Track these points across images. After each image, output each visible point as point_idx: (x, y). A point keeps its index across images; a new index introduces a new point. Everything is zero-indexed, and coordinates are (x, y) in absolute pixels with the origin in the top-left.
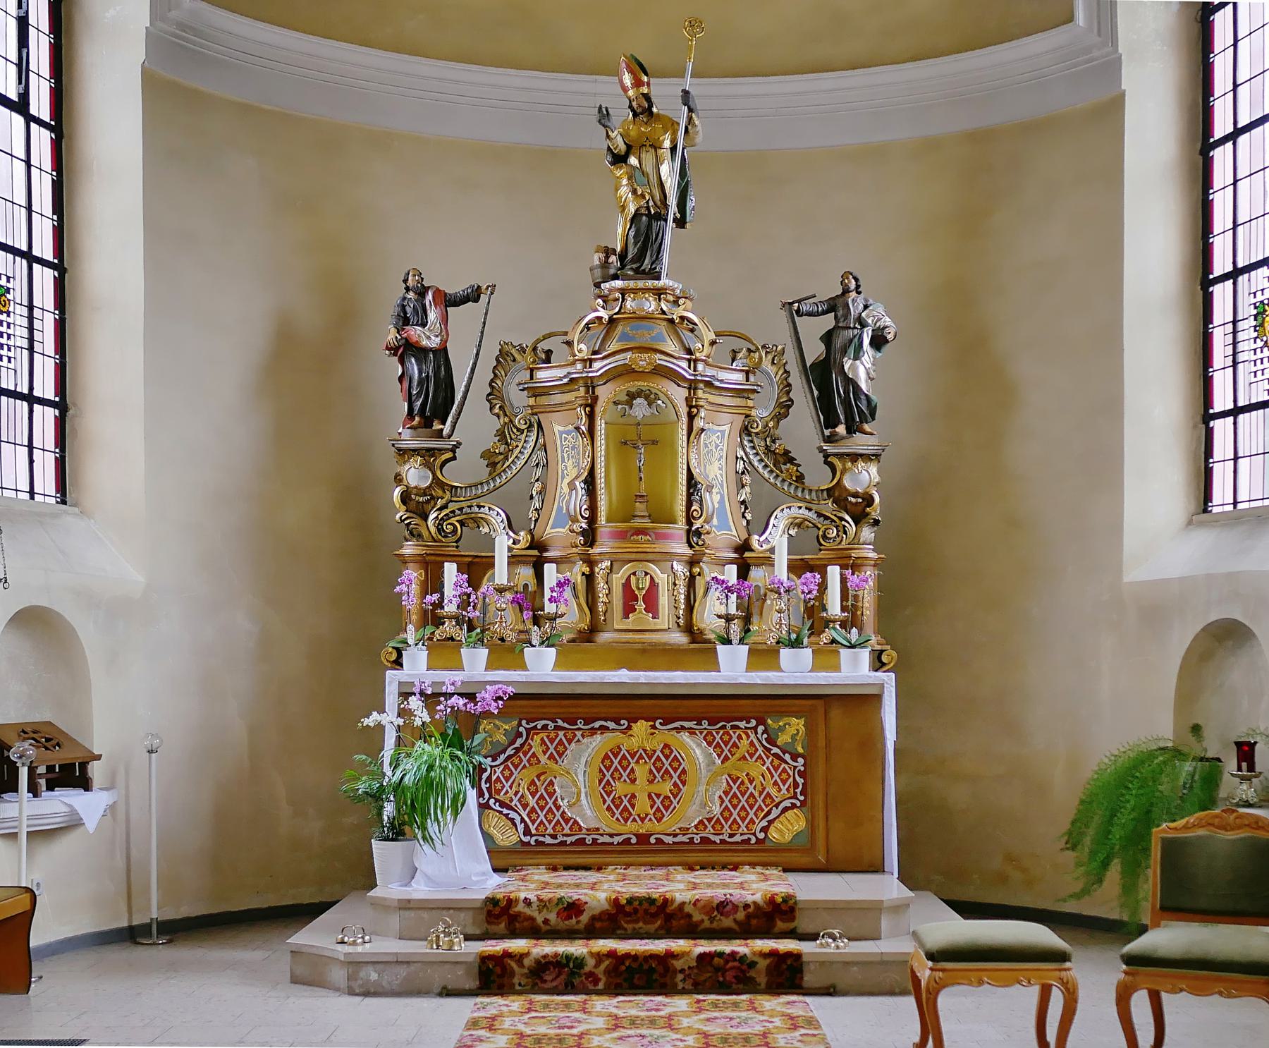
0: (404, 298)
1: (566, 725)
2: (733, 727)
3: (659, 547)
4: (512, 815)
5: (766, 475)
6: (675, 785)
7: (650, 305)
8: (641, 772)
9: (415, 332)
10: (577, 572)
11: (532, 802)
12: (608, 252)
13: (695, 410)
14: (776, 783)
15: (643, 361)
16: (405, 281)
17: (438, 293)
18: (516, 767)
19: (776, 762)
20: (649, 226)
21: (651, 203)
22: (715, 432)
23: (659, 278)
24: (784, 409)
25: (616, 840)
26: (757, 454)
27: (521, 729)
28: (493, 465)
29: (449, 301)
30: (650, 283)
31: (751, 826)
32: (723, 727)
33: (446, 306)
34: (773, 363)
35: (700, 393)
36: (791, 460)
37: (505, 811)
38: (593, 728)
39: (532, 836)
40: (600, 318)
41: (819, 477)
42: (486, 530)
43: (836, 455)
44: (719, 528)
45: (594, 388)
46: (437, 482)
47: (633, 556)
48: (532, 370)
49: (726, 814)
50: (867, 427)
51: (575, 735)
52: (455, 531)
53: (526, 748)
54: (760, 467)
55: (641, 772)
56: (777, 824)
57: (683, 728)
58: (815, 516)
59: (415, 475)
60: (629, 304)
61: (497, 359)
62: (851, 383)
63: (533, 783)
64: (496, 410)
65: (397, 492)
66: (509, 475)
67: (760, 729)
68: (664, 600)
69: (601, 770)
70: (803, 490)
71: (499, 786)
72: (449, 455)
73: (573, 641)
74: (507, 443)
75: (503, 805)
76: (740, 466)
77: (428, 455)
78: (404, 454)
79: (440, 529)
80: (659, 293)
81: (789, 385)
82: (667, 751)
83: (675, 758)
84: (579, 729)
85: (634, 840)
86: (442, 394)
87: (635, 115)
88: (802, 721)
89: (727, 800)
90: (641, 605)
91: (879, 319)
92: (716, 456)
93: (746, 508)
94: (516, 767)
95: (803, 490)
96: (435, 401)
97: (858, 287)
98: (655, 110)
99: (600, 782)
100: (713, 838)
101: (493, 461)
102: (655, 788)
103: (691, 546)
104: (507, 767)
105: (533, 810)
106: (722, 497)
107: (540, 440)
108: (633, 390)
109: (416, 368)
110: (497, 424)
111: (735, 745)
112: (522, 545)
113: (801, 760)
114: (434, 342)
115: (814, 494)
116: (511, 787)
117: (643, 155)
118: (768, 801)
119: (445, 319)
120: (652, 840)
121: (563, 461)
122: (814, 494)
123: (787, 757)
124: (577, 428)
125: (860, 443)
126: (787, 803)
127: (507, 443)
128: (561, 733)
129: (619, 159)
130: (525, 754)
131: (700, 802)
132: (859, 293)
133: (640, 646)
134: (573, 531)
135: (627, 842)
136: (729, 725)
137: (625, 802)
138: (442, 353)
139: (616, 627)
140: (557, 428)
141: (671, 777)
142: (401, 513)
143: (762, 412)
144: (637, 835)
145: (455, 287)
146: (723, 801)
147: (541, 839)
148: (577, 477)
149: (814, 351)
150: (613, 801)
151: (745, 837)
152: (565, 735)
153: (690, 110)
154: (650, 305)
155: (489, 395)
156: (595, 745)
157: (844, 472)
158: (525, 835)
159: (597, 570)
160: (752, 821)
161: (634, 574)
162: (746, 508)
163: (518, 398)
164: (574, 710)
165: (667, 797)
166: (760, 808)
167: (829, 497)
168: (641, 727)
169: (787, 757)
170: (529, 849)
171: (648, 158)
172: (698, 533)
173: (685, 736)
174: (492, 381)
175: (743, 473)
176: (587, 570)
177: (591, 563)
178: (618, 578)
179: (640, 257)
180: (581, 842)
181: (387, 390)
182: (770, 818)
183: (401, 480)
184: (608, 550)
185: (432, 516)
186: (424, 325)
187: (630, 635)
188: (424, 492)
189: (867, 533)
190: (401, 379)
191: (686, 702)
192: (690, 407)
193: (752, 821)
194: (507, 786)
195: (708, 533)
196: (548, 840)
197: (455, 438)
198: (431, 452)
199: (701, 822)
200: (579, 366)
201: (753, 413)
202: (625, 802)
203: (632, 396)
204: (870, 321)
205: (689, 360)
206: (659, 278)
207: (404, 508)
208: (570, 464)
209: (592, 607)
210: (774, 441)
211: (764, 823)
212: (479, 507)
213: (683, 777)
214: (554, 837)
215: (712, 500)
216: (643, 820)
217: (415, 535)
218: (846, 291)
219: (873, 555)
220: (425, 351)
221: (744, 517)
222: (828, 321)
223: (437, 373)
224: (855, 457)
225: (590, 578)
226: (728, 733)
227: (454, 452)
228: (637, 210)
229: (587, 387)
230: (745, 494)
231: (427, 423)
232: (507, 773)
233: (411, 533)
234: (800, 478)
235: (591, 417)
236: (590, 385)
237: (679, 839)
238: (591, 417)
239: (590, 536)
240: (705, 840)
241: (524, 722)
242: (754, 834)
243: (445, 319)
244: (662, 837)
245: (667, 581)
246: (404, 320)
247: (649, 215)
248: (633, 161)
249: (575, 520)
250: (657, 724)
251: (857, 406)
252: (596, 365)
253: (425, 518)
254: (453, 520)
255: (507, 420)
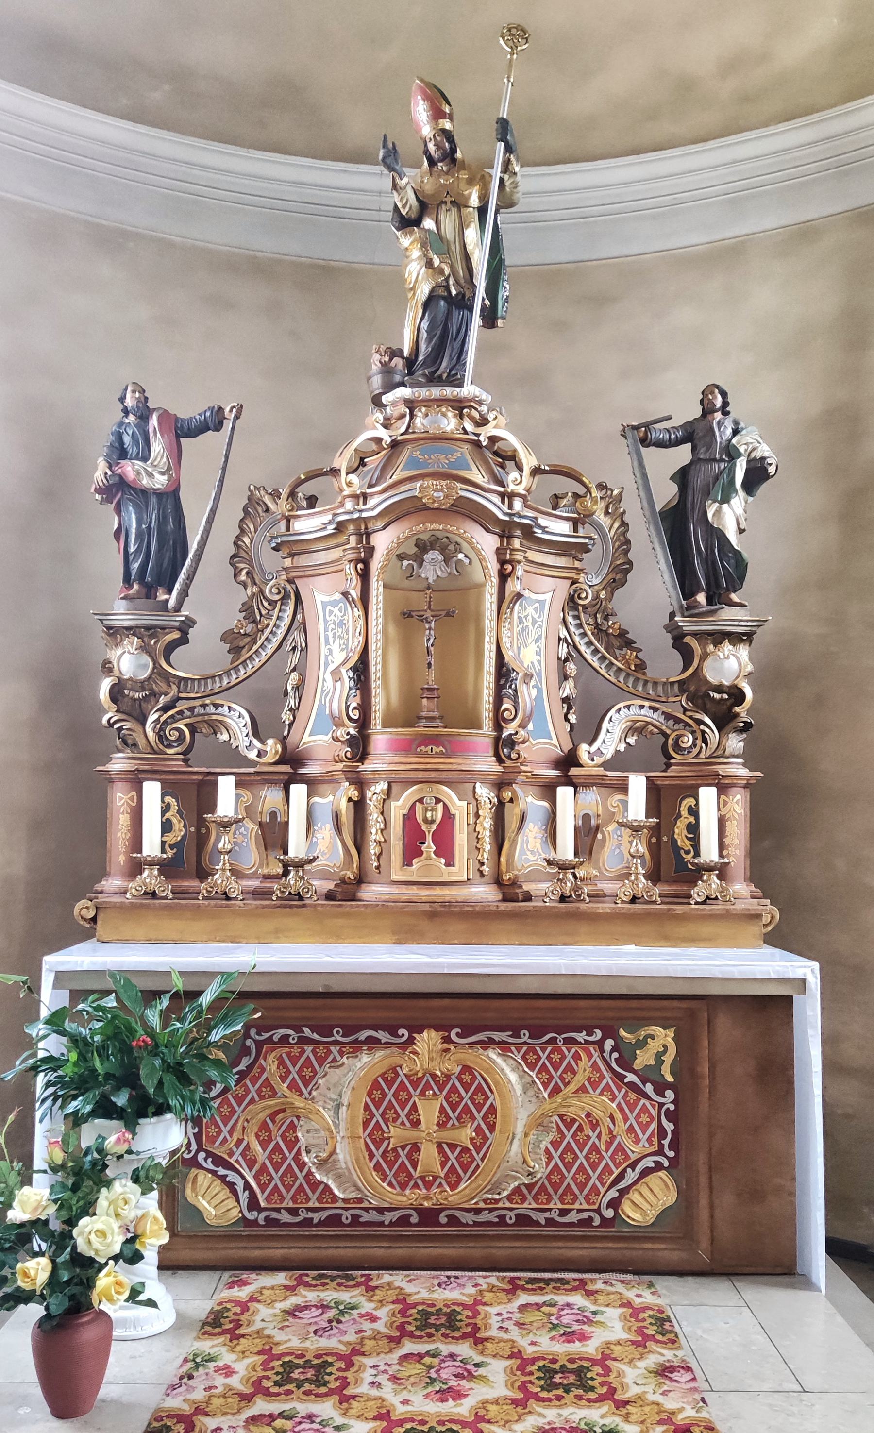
0: (121, 424)
1: (316, 1036)
2: (567, 1041)
3: (457, 763)
4: (232, 1177)
5: (596, 664)
6: (478, 1130)
7: (449, 423)
8: (429, 1111)
9: (130, 469)
10: (341, 797)
11: (261, 1154)
12: (395, 353)
13: (509, 567)
14: (631, 1129)
15: (434, 492)
16: (122, 399)
17: (165, 417)
18: (240, 1102)
19: (632, 1096)
20: (448, 316)
21: (451, 281)
22: (532, 602)
23: (461, 385)
24: (619, 574)
25: (388, 1217)
26: (584, 634)
27: (249, 1042)
28: (236, 651)
29: (182, 431)
30: (449, 391)
31: (593, 1198)
32: (553, 1041)
33: (178, 437)
34: (607, 513)
35: (516, 543)
36: (629, 644)
37: (222, 1171)
38: (356, 1041)
39: (260, 1210)
40: (378, 441)
41: (667, 665)
42: (224, 737)
43: (695, 634)
44: (537, 734)
45: (368, 535)
46: (158, 670)
47: (421, 775)
48: (288, 521)
49: (555, 1178)
50: (734, 597)
51: (329, 1052)
52: (181, 738)
53: (256, 1071)
54: (587, 653)
55: (429, 1111)
56: (634, 1196)
57: (491, 1041)
58: (662, 719)
59: (129, 661)
60: (420, 421)
61: (245, 510)
62: (716, 535)
63: (264, 1126)
64: (243, 577)
65: (106, 685)
66: (257, 663)
67: (609, 1044)
68: (461, 838)
69: (367, 1107)
70: (646, 682)
71: (213, 1131)
72: (176, 635)
73: (330, 896)
74: (254, 621)
75: (219, 1161)
76: (563, 651)
77: (146, 634)
78: (114, 633)
79: (161, 736)
80: (460, 406)
81: (628, 542)
82: (467, 1077)
83: (479, 1088)
84: (336, 1042)
85: (414, 1219)
86: (168, 555)
87: (432, 162)
88: (671, 1033)
89: (556, 1156)
90: (429, 847)
91: (754, 449)
92: (533, 635)
93: (569, 708)
94: (240, 1102)
95: (646, 682)
96: (160, 562)
97: (725, 404)
98: (459, 155)
99: (366, 1124)
100: (534, 1215)
101: (237, 644)
102: (448, 1136)
103: (500, 761)
104: (226, 1102)
105: (263, 1169)
106: (540, 691)
107: (299, 617)
108: (425, 537)
109: (133, 517)
110: (243, 595)
111: (570, 1069)
112: (270, 758)
113: (670, 1095)
114: (160, 481)
115: (660, 688)
116: (231, 1133)
117: (442, 217)
118: (620, 1157)
119: (177, 454)
120: (443, 1219)
121: (327, 642)
122: (660, 688)
123: (649, 1088)
124: (345, 594)
125: (730, 617)
126: (649, 1162)
127: (254, 621)
128: (309, 1049)
129: (407, 223)
130: (254, 1082)
131: (520, 1148)
132: (726, 413)
133: (426, 907)
134: (336, 739)
135: (404, 1221)
136: (560, 1039)
137: (403, 1157)
138: (170, 499)
139: (394, 877)
140: (320, 598)
141: (473, 1118)
142: (110, 714)
143: (592, 581)
144: (420, 1211)
145: (189, 409)
146: (550, 1158)
147: (274, 1215)
148: (343, 663)
149: (666, 492)
150: (384, 1155)
151: (585, 1215)
152: (314, 1052)
153: (509, 149)
154: (449, 423)
155: (233, 557)
156: (364, 1065)
157: (705, 656)
158: (250, 1209)
159: (369, 794)
160: (595, 1189)
161: (421, 801)
162: (569, 708)
163: (270, 561)
164: (326, 1014)
165: (465, 1150)
166: (607, 1170)
167: (682, 691)
168: (428, 1041)
169: (649, 1088)
170: (255, 1231)
171: (449, 222)
172: (511, 743)
173: (493, 1054)
174: (238, 538)
175: (566, 660)
176: (355, 794)
177: (360, 783)
178: (398, 808)
179: (436, 356)
180: (334, 1220)
181: (102, 547)
182: (622, 1185)
183: (111, 670)
184: (385, 767)
185: (152, 717)
186: (145, 459)
187: (414, 890)
188: (142, 685)
189: (735, 743)
190: (117, 534)
191: (496, 1003)
192: (502, 562)
193: (595, 1190)
194: (225, 1130)
195: (524, 742)
196: (285, 1217)
197: (185, 612)
198: (152, 630)
199: (517, 1191)
200: (349, 505)
201: (582, 578)
202: (403, 1157)
203: (423, 547)
204: (742, 449)
205: (502, 495)
206: (461, 385)
207: (114, 707)
208: (335, 647)
209: (360, 843)
210: (606, 618)
211: (613, 1194)
212: (216, 706)
213: (491, 1118)
214: (293, 1212)
215: (527, 694)
216: (428, 1185)
217: (127, 743)
218: (707, 411)
219: (743, 772)
220: (144, 493)
221: (567, 719)
222: (683, 454)
223: (162, 522)
224: (719, 637)
225: (359, 806)
226: (560, 1052)
227: (705, 901)
228: (432, 291)
229: (359, 535)
230: (569, 688)
231: (149, 592)
232: (225, 1110)
233: (125, 742)
234: (641, 667)
235: (365, 576)
236: (365, 535)
237: (484, 1217)
238: (365, 576)
239: (360, 746)
240: (523, 1220)
241: (253, 1032)
242: (598, 1211)
243: (177, 454)
244: (457, 1213)
245: (467, 811)
246: (119, 452)
247: (448, 298)
248: (428, 223)
249: (339, 724)
250: (453, 1037)
251: (723, 566)
252: (371, 502)
253: (143, 721)
254: (180, 725)
255: (255, 589)
